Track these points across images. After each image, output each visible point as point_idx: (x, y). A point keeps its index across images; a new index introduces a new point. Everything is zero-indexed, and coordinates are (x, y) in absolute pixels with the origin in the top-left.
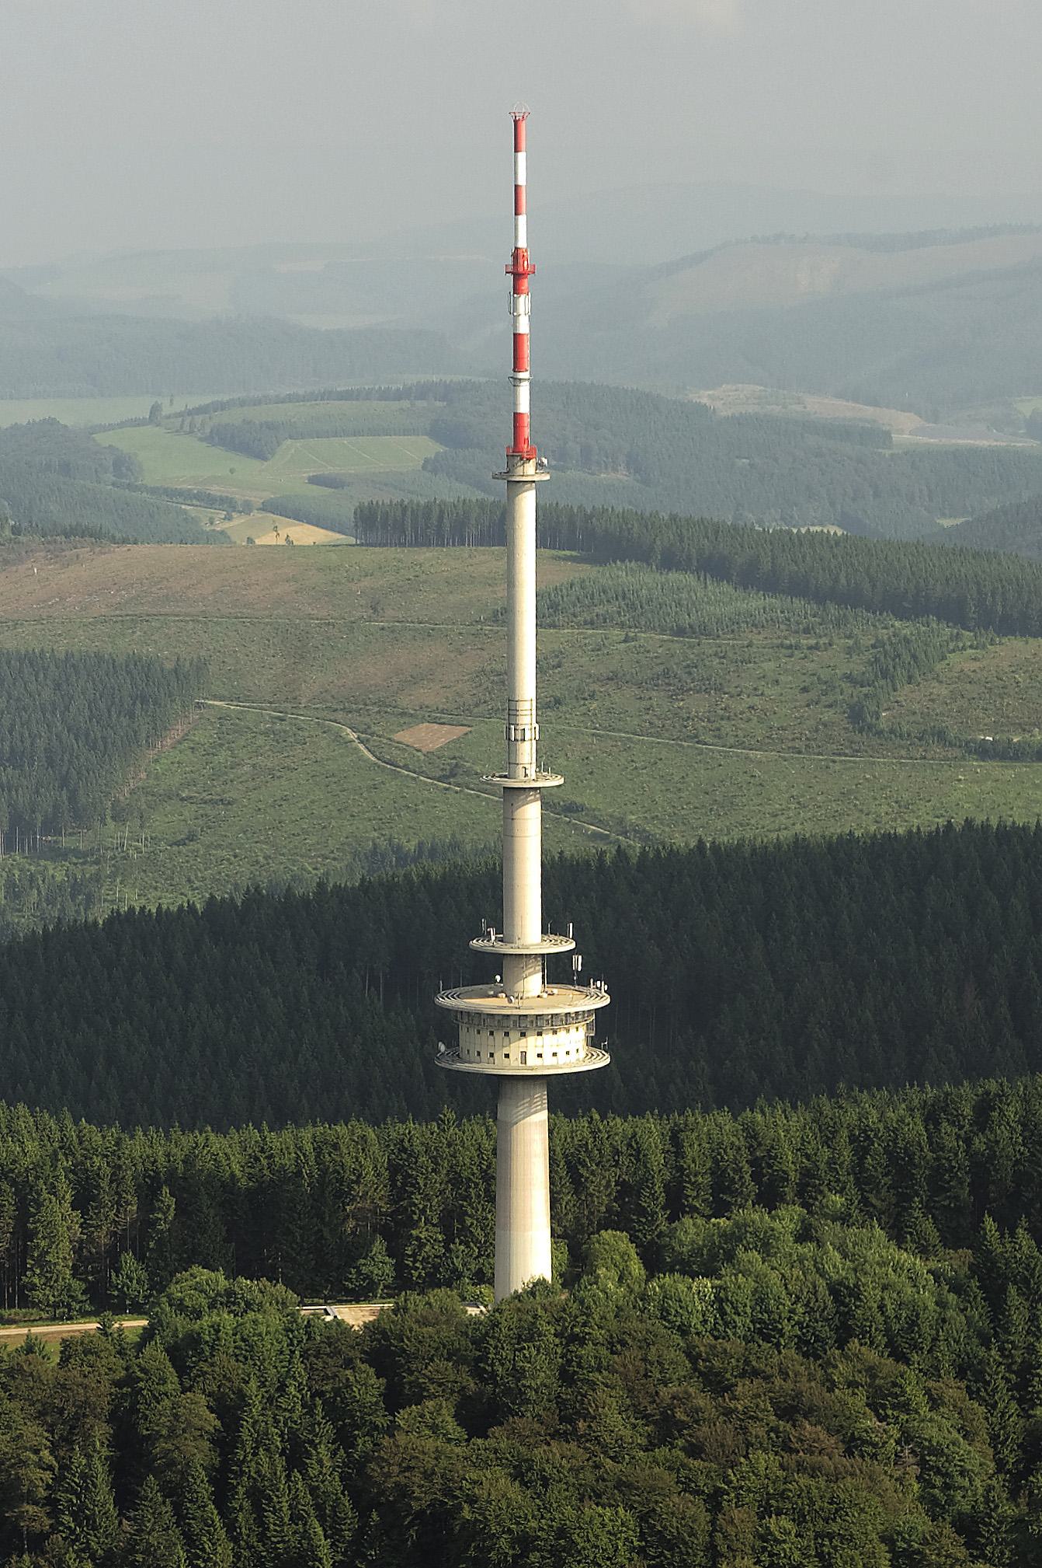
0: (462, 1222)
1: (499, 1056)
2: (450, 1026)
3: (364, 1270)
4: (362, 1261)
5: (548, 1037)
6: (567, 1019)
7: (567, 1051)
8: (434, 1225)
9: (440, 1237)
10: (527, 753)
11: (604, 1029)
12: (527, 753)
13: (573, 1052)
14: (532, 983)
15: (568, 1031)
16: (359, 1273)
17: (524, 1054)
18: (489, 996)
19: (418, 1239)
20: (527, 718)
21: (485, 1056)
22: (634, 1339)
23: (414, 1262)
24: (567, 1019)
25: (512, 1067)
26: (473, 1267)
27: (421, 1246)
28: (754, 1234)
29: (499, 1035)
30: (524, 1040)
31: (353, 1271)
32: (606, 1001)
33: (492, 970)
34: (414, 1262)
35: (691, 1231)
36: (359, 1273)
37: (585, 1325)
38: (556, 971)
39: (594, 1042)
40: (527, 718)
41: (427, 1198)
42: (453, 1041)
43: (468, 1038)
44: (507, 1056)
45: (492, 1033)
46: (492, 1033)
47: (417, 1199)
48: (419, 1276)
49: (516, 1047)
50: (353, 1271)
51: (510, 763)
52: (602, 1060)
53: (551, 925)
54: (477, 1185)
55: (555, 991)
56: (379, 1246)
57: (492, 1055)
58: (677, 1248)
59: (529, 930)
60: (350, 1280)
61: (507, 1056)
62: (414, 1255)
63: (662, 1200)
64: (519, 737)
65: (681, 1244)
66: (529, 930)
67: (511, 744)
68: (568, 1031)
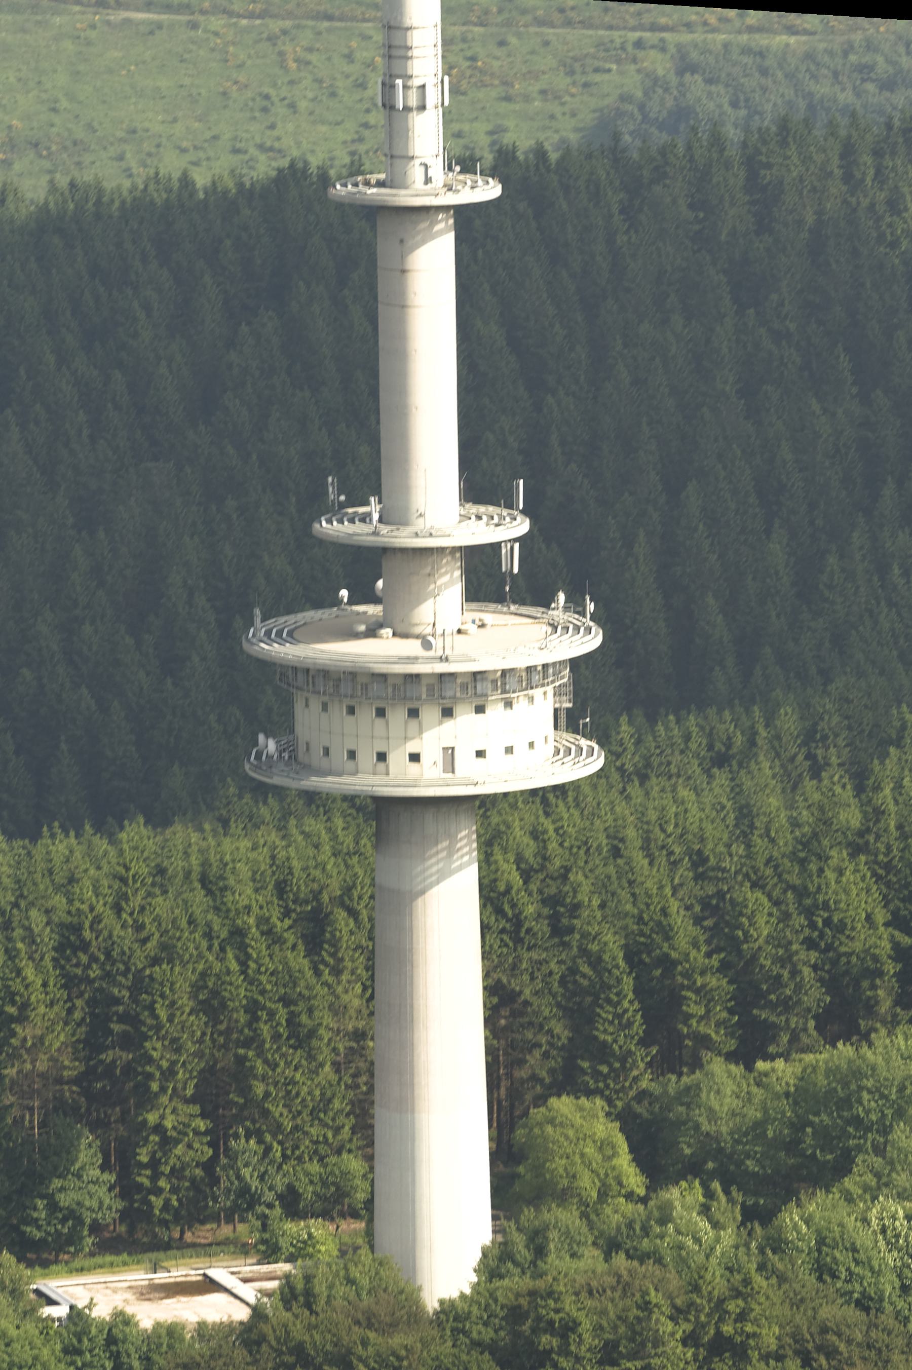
0: (245, 1090)
1: (397, 759)
2: (275, 695)
3: (64, 1200)
4: (57, 1183)
5: (465, 719)
6: (507, 683)
7: (518, 748)
8: (187, 1101)
9: (202, 1125)
10: (426, 136)
11: (592, 699)
12: (426, 136)
13: (521, 748)
14: (444, 602)
15: (509, 704)
16: (53, 1207)
17: (449, 754)
18: (357, 636)
19: (159, 1129)
20: (426, 63)
21: (366, 758)
22: (849, 1342)
23: (154, 1178)
24: (507, 683)
25: (428, 780)
26: (280, 1183)
27: (167, 1142)
28: (878, 1092)
29: (397, 716)
30: (449, 724)
31: (40, 1204)
32: (593, 641)
33: (371, 576)
34: (154, 1178)
35: (724, 1093)
36: (53, 1207)
37: (742, 1317)
38: (486, 577)
39: (568, 721)
40: (426, 63)
41: (176, 1046)
42: (282, 725)
43: (312, 721)
44: (415, 758)
45: (325, 707)
46: (381, 713)
47: (155, 1048)
48: (166, 1206)
49: (434, 737)
50: (40, 1204)
51: (395, 156)
52: (585, 763)
53: (479, 485)
54: (272, 1014)
55: (488, 618)
56: (87, 1152)
57: (382, 757)
58: (705, 1127)
59: (434, 498)
60: (35, 1222)
61: (415, 758)
62: (154, 1164)
63: (638, 1027)
64: (413, 101)
65: (712, 1116)
66: (434, 498)
67: (393, 116)
68: (509, 704)
